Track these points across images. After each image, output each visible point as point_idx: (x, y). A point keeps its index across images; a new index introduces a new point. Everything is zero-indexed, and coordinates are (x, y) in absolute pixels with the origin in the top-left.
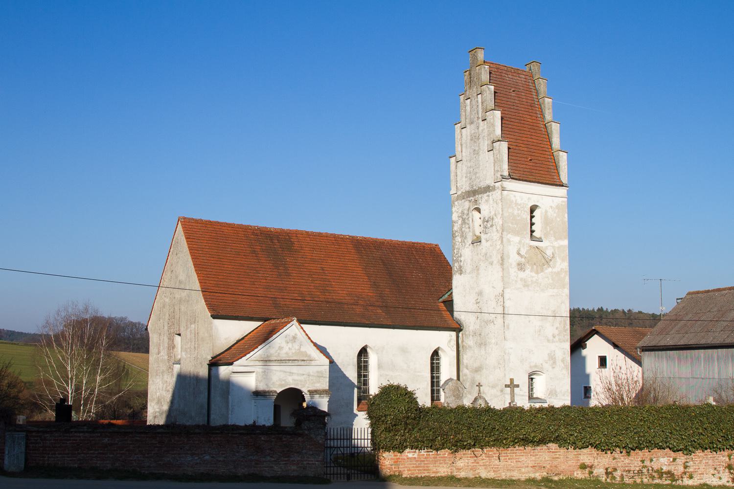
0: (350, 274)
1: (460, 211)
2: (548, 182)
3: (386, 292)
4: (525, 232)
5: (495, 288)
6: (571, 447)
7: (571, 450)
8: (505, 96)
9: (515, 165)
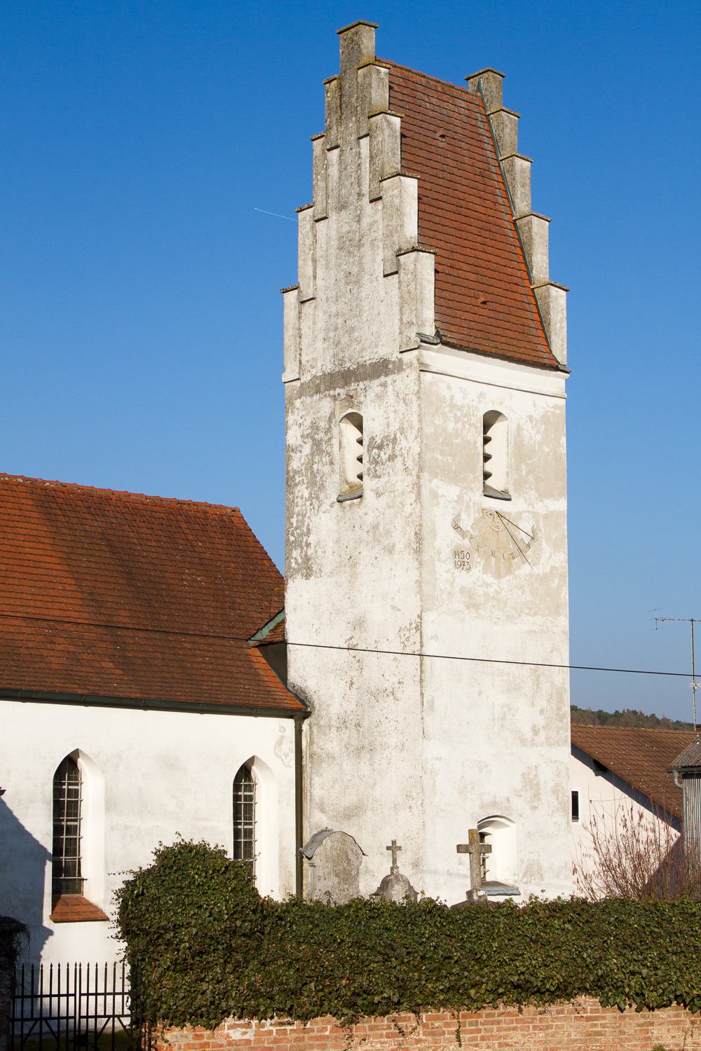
0: (31, 570)
1: (308, 423)
2: (524, 357)
3: (121, 619)
4: (471, 476)
5: (399, 610)
6: (630, 1006)
7: (630, 1011)
8: (423, 146)
9: (449, 311)
